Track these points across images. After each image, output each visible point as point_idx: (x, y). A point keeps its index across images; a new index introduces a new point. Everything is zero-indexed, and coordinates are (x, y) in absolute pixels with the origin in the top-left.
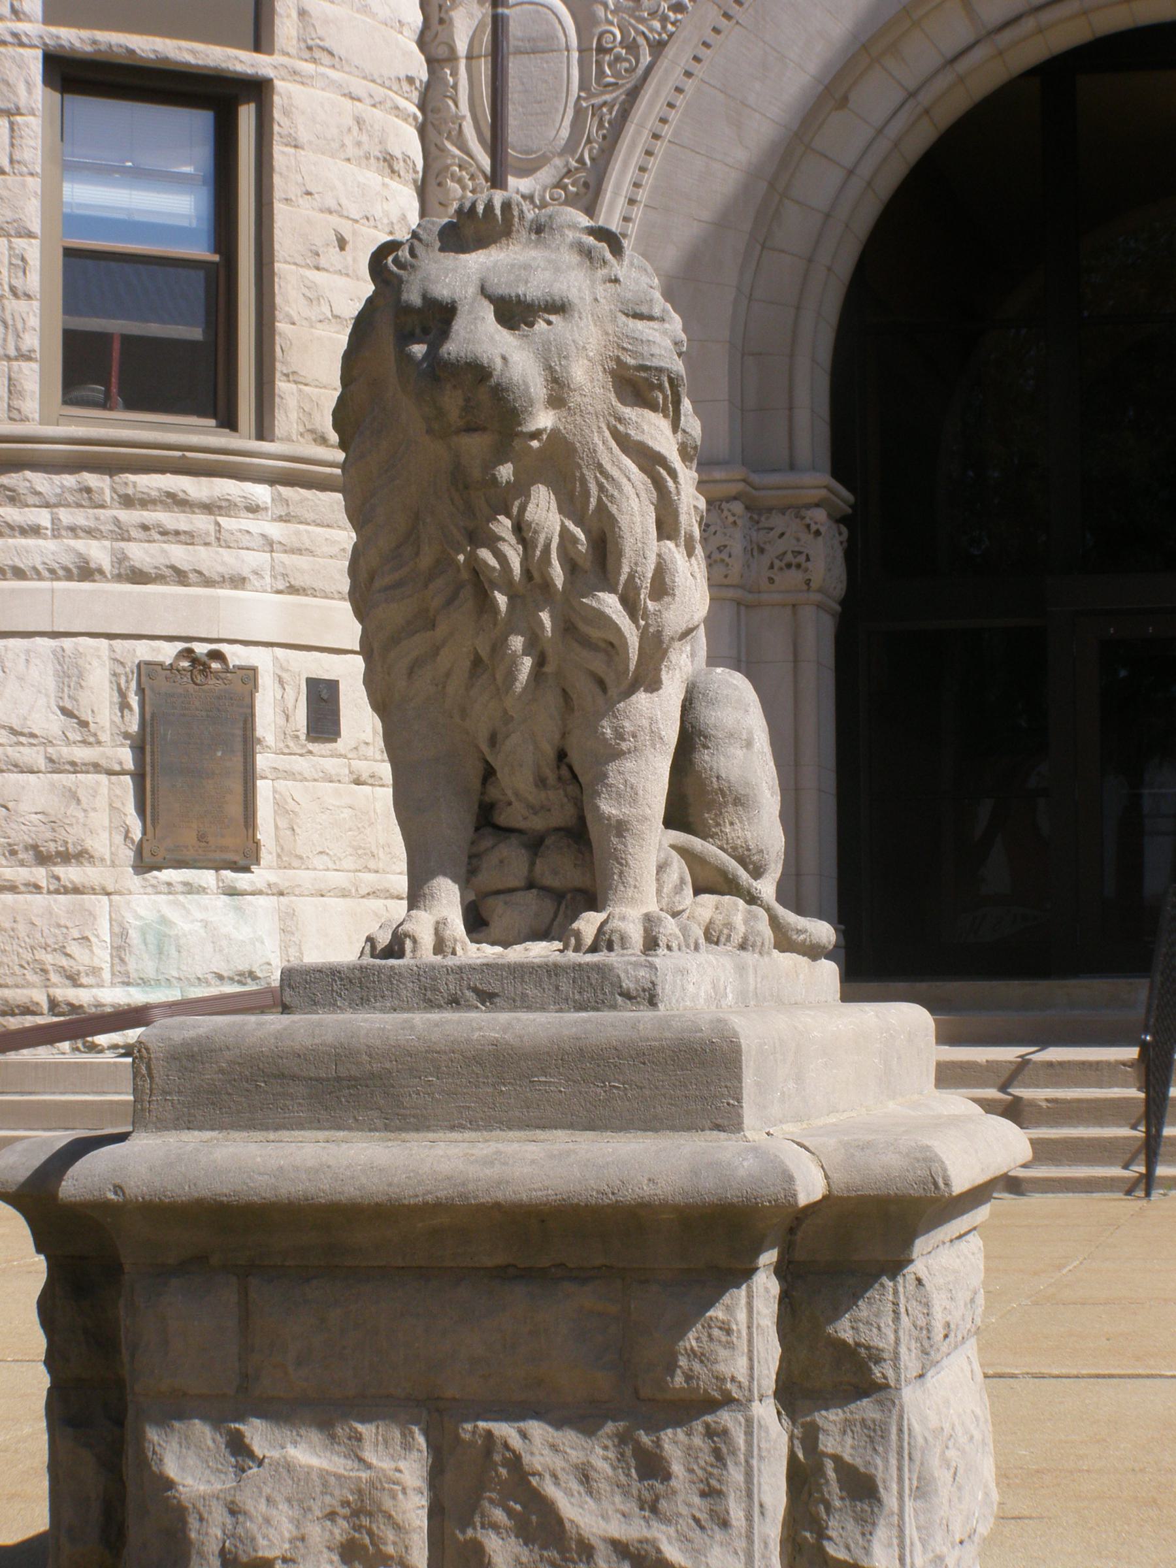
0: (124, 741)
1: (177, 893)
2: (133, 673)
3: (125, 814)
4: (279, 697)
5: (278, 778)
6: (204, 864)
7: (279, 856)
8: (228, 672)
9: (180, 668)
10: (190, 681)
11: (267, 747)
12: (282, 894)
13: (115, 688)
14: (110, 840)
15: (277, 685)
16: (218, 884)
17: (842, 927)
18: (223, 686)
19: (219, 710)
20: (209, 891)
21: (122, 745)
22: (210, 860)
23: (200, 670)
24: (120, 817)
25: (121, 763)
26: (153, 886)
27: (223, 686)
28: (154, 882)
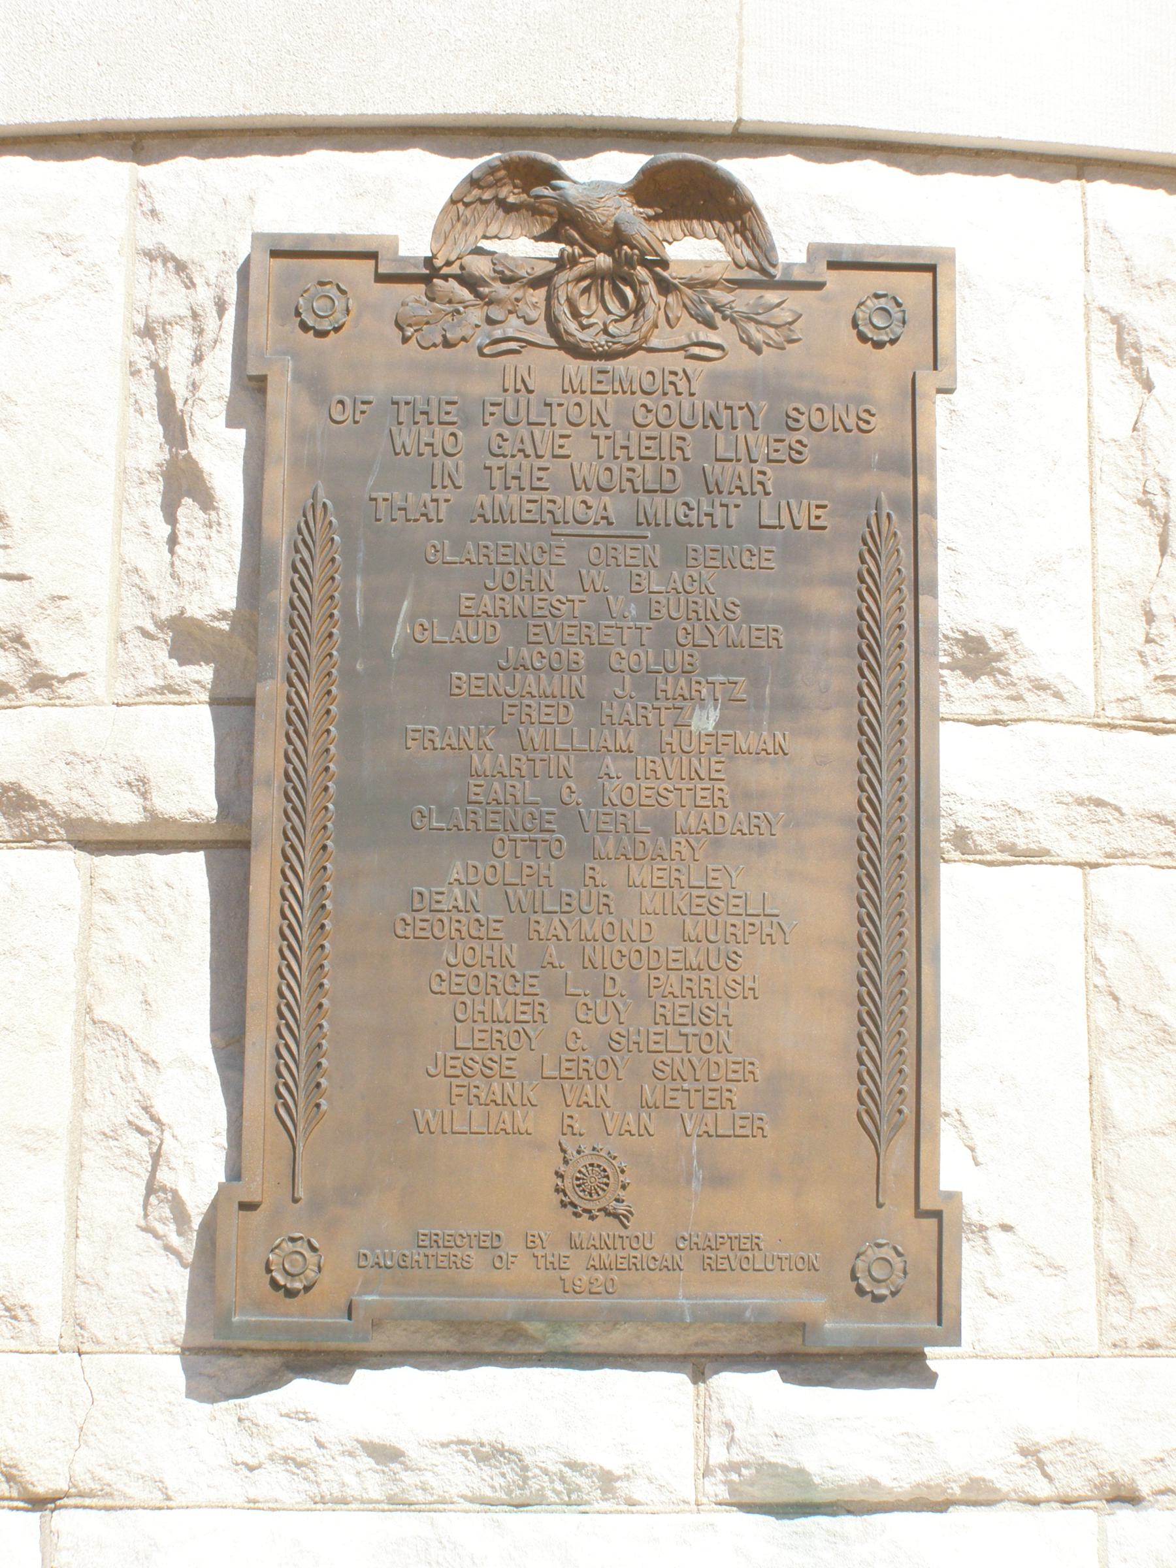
0: (173, 666)
1: (442, 1503)
2: (221, 308)
3: (150, 1062)
4: (1115, 425)
5: (1116, 856)
6: (615, 1339)
7: (1113, 1281)
8: (769, 283)
9: (480, 267)
10: (540, 334)
11: (1040, 686)
12: (1126, 1497)
13: (149, 397)
14: (74, 1200)
15: (1109, 367)
16: (701, 1446)
17: (641, 176)
18: (740, 359)
19: (712, 488)
20: (638, 1490)
21: (170, 690)
22: (666, 1318)
23: (596, 276)
24: (128, 1077)
25: (141, 786)
26: (295, 1463)
27: (740, 359)
28: (296, 1439)
